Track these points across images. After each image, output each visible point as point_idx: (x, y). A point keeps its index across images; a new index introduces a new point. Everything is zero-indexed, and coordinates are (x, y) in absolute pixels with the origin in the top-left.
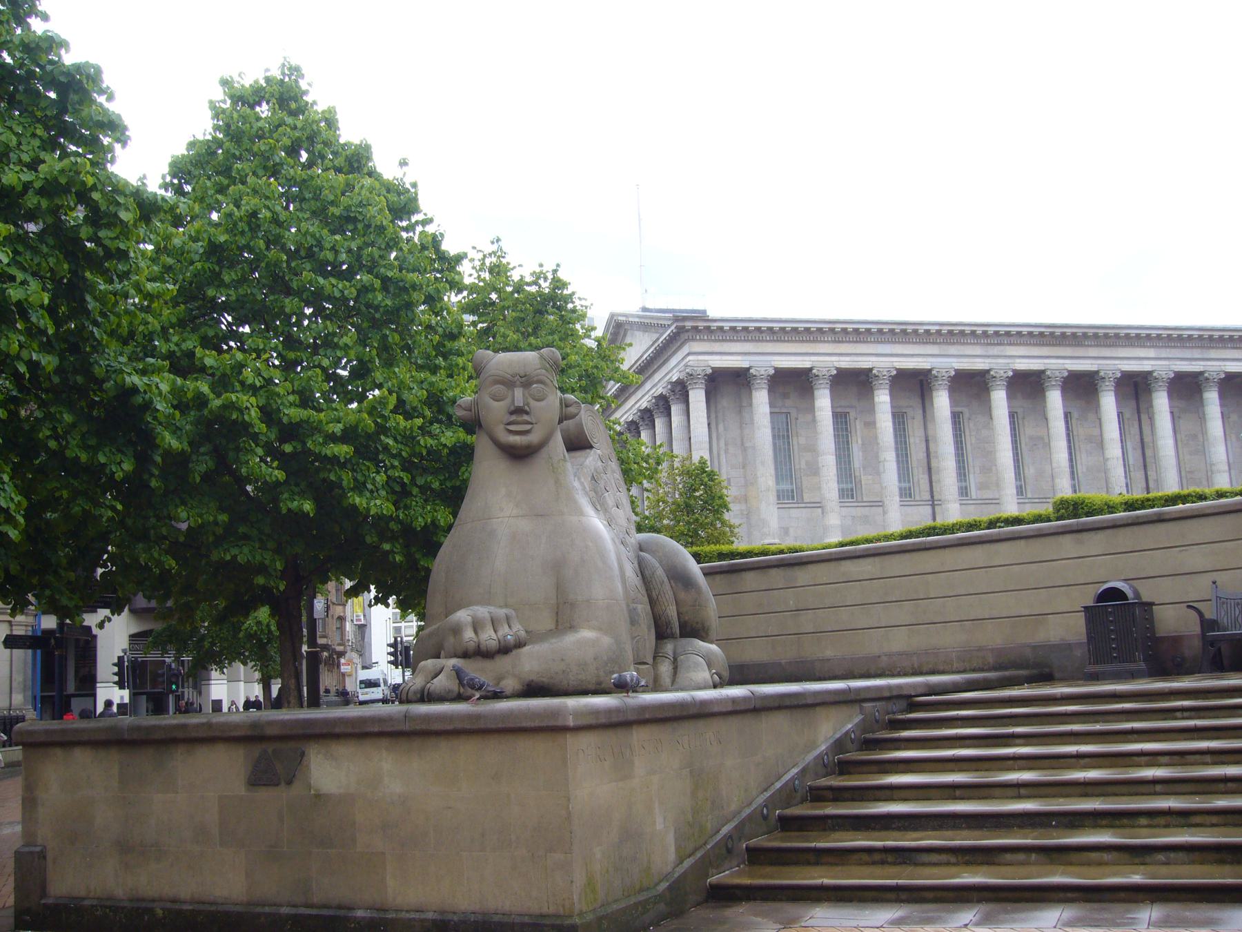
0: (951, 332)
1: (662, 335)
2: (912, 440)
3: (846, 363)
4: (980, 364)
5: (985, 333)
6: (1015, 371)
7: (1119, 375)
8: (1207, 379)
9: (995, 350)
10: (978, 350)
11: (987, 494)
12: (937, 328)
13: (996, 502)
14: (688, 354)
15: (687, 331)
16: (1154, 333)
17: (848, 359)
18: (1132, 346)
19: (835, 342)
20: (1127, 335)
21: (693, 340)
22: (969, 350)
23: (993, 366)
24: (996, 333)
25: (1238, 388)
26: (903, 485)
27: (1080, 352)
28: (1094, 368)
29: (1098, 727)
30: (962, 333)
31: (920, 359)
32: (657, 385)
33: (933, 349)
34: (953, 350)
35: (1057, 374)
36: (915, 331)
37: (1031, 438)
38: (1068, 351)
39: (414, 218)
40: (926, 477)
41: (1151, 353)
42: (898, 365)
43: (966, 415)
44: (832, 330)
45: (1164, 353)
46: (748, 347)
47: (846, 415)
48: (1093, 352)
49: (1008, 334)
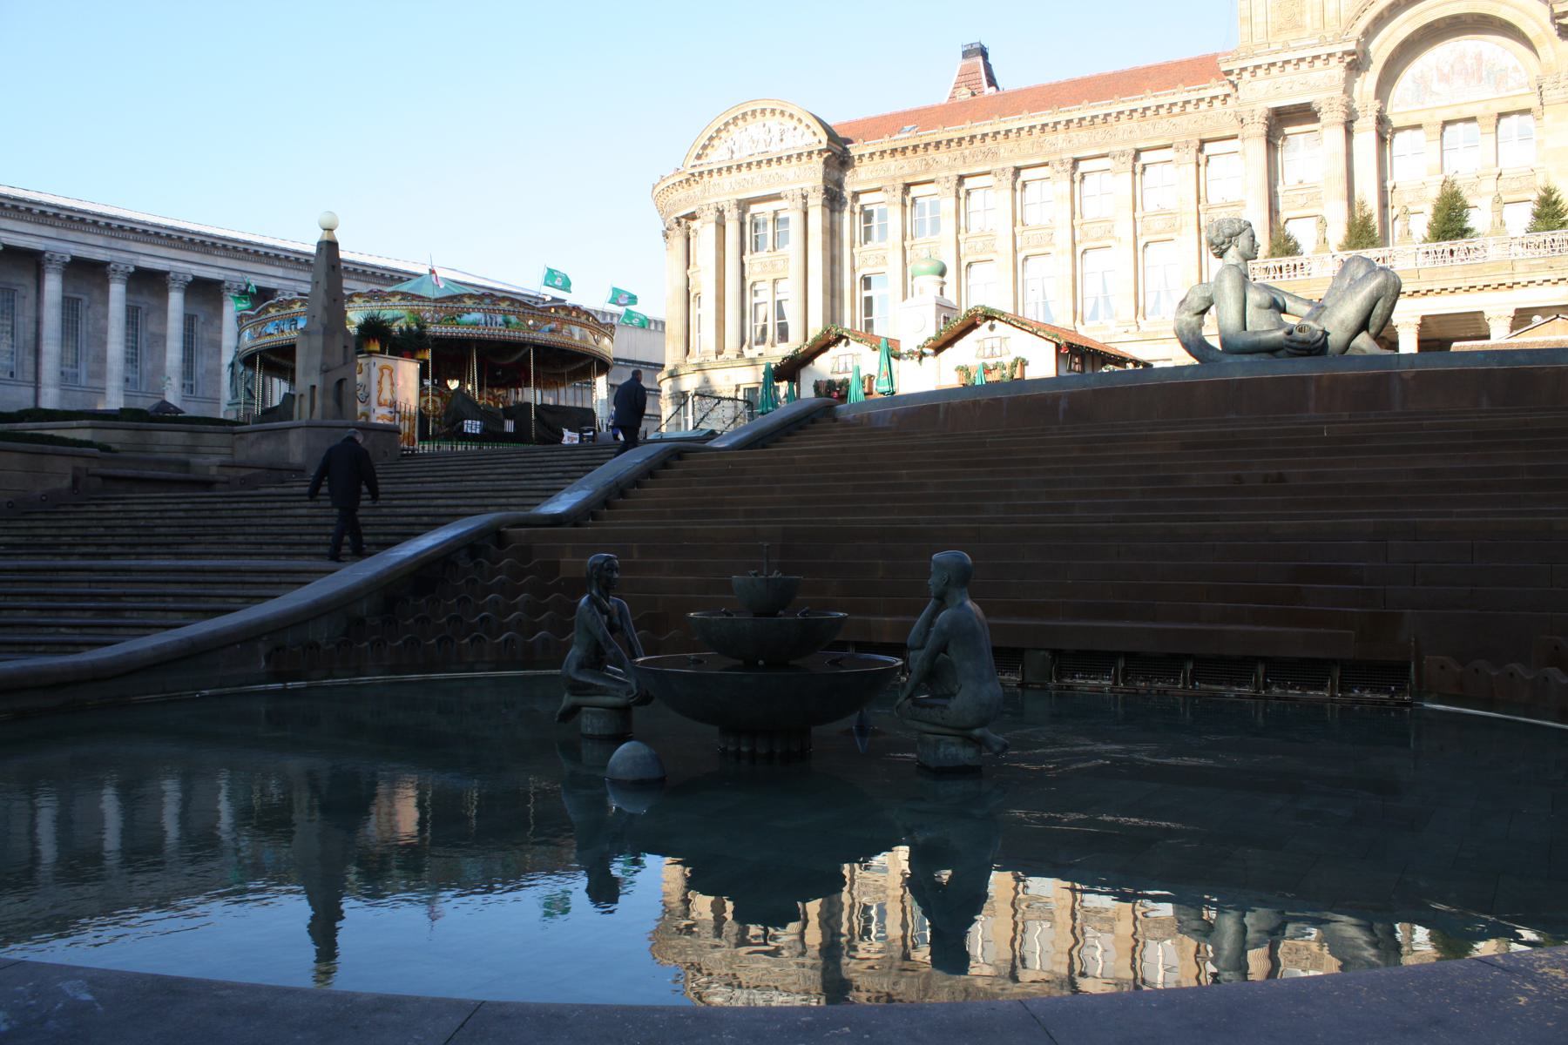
0: (70, 218)
2: (20, 319)
4: (100, 255)
5: (108, 225)
6: (137, 268)
9: (120, 244)
10: (101, 241)
11: (95, 383)
13: (102, 392)
16: (283, 254)
18: (208, 253)
20: (256, 252)
22: (90, 239)
24: (121, 227)
26: (1063, 404)
28: (221, 278)
29: (264, 579)
30: (83, 220)
34: (72, 236)
36: (29, 210)
37: (153, 334)
38: (196, 257)
40: (32, 358)
41: (280, 272)
42: (196, 273)
43: (202, 319)
45: (292, 274)
47: (137, 309)
48: (222, 262)
49: (133, 230)
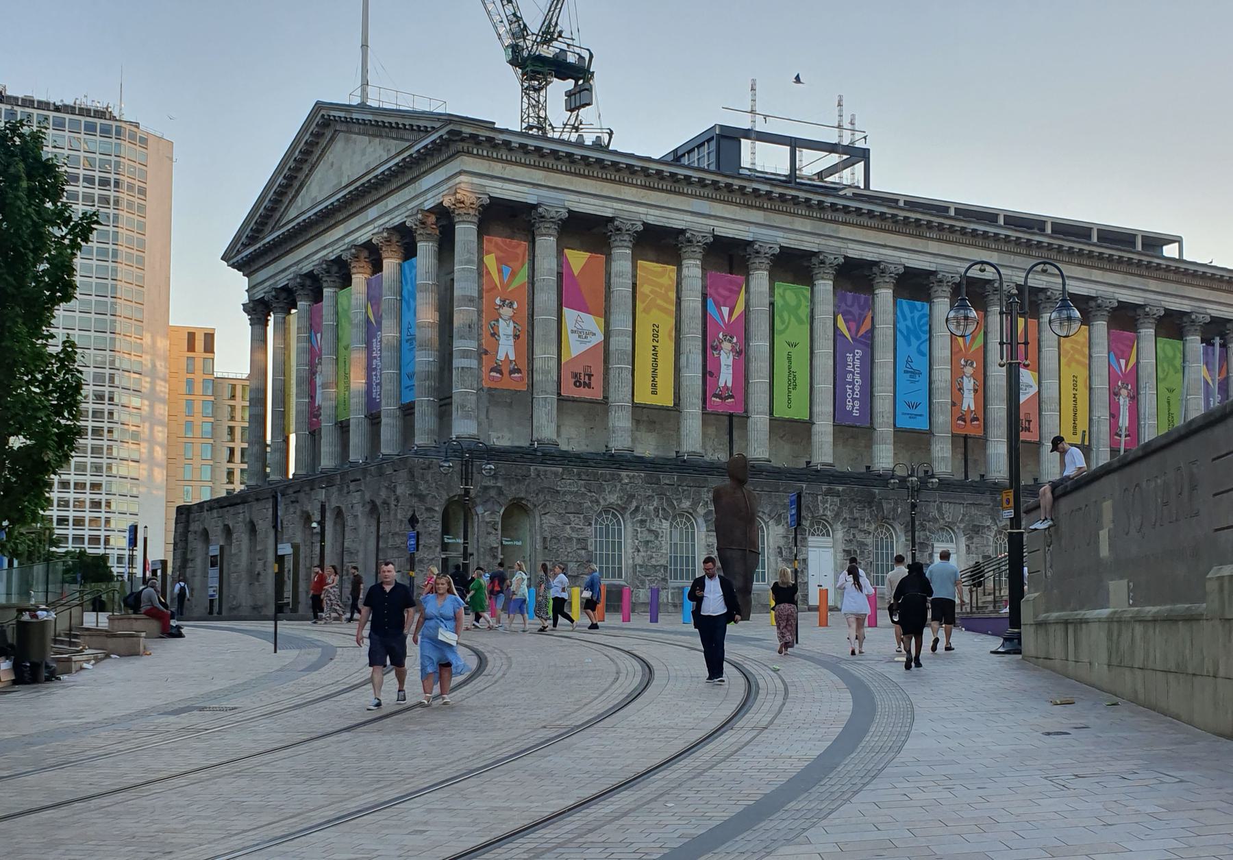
1: (416, 142)
3: (654, 217)
4: (809, 244)
7: (902, 270)
8: (689, 241)
9: (829, 228)
10: (807, 225)
12: (768, 188)
14: (460, 173)
15: (463, 140)
17: (657, 212)
19: (644, 187)
21: (469, 153)
23: (822, 248)
25: (1216, 330)
27: (919, 244)
31: (741, 227)
32: (368, 225)
33: (757, 216)
34: (778, 219)
35: (892, 269)
36: (742, 188)
39: (957, 601)
44: (645, 170)
46: (538, 176)
48: (933, 247)
